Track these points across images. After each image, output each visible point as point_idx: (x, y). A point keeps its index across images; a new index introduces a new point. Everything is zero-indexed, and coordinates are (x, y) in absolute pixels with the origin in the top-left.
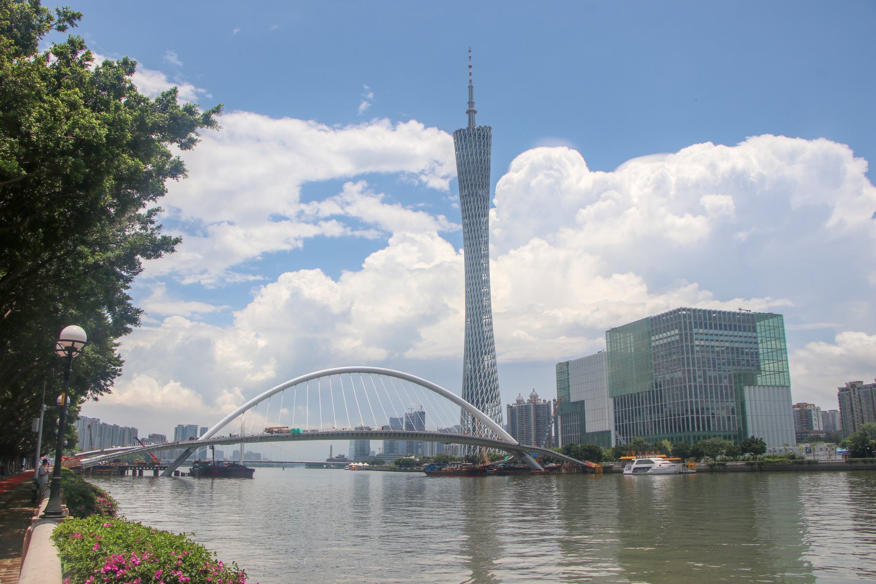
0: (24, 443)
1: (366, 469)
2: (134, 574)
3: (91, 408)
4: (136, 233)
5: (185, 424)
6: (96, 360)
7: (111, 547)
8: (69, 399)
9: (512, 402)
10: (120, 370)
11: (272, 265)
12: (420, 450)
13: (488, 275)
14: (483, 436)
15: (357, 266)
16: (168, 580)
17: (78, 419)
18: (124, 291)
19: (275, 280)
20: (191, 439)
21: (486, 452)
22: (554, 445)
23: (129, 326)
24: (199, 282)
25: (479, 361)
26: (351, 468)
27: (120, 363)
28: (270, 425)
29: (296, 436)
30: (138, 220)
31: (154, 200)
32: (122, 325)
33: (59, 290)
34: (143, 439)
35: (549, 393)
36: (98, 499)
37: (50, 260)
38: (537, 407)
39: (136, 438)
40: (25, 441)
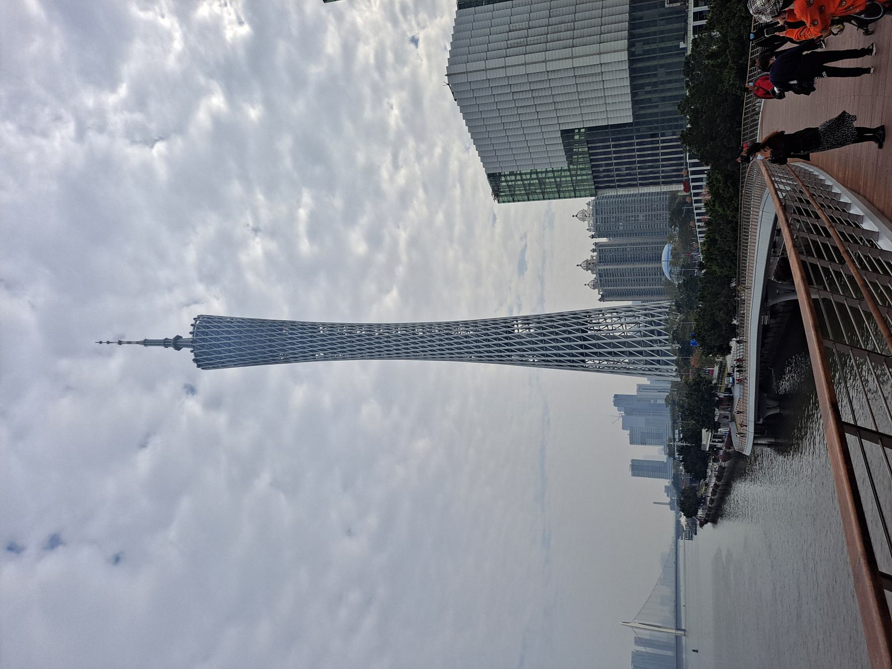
9: (596, 294)
38: (602, 259)
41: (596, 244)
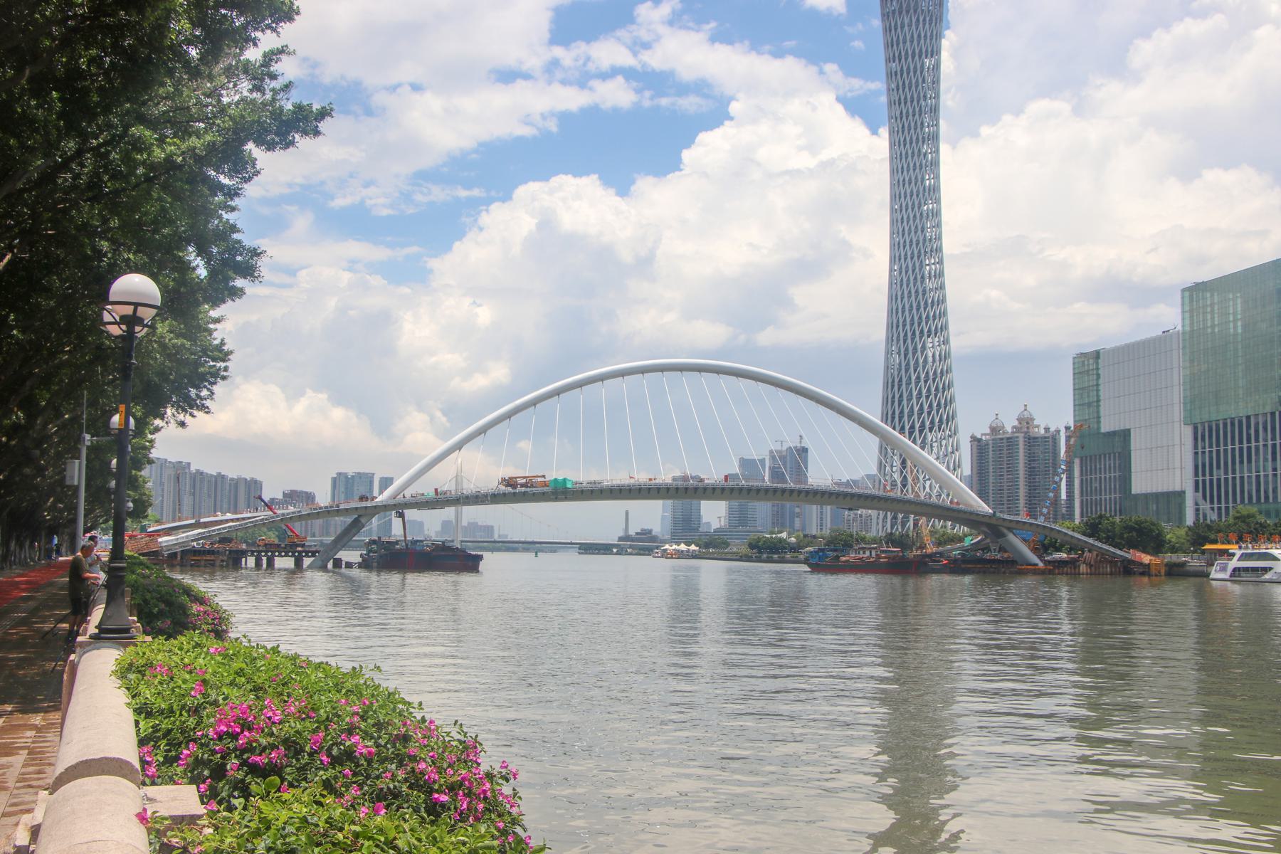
0: (53, 508)
1: (694, 556)
2: (271, 740)
3: (175, 440)
4: (243, 100)
5: (351, 470)
6: (179, 349)
7: (225, 690)
8: (132, 420)
9: (982, 430)
10: (226, 369)
11: (498, 168)
12: (797, 522)
13: (937, 177)
14: (922, 495)
15: (667, 164)
16: (335, 751)
17: (151, 462)
18: (225, 216)
19: (506, 197)
20: (362, 498)
21: (927, 527)
22: (1063, 517)
23: (239, 282)
24: (362, 202)
25: (915, 349)
26: (665, 555)
27: (225, 356)
28: (510, 472)
29: (560, 492)
30: (246, 72)
31: (274, 30)
32: (227, 279)
33: (100, 213)
34: (272, 500)
35: (1056, 415)
36: (195, 608)
37: (79, 153)
38: (1031, 441)
39: (260, 498)
40: (54, 503)
41: (1058, 431)
